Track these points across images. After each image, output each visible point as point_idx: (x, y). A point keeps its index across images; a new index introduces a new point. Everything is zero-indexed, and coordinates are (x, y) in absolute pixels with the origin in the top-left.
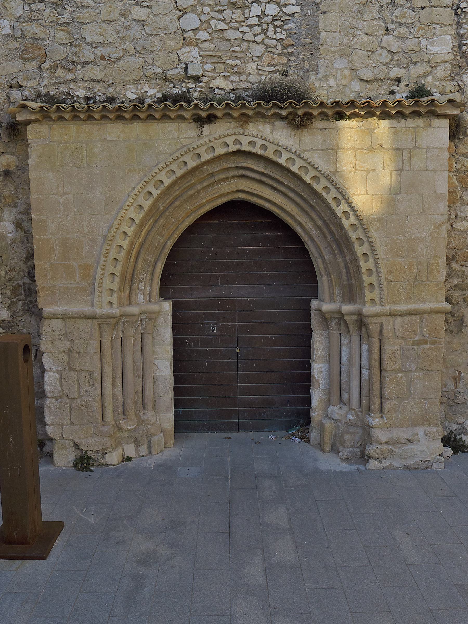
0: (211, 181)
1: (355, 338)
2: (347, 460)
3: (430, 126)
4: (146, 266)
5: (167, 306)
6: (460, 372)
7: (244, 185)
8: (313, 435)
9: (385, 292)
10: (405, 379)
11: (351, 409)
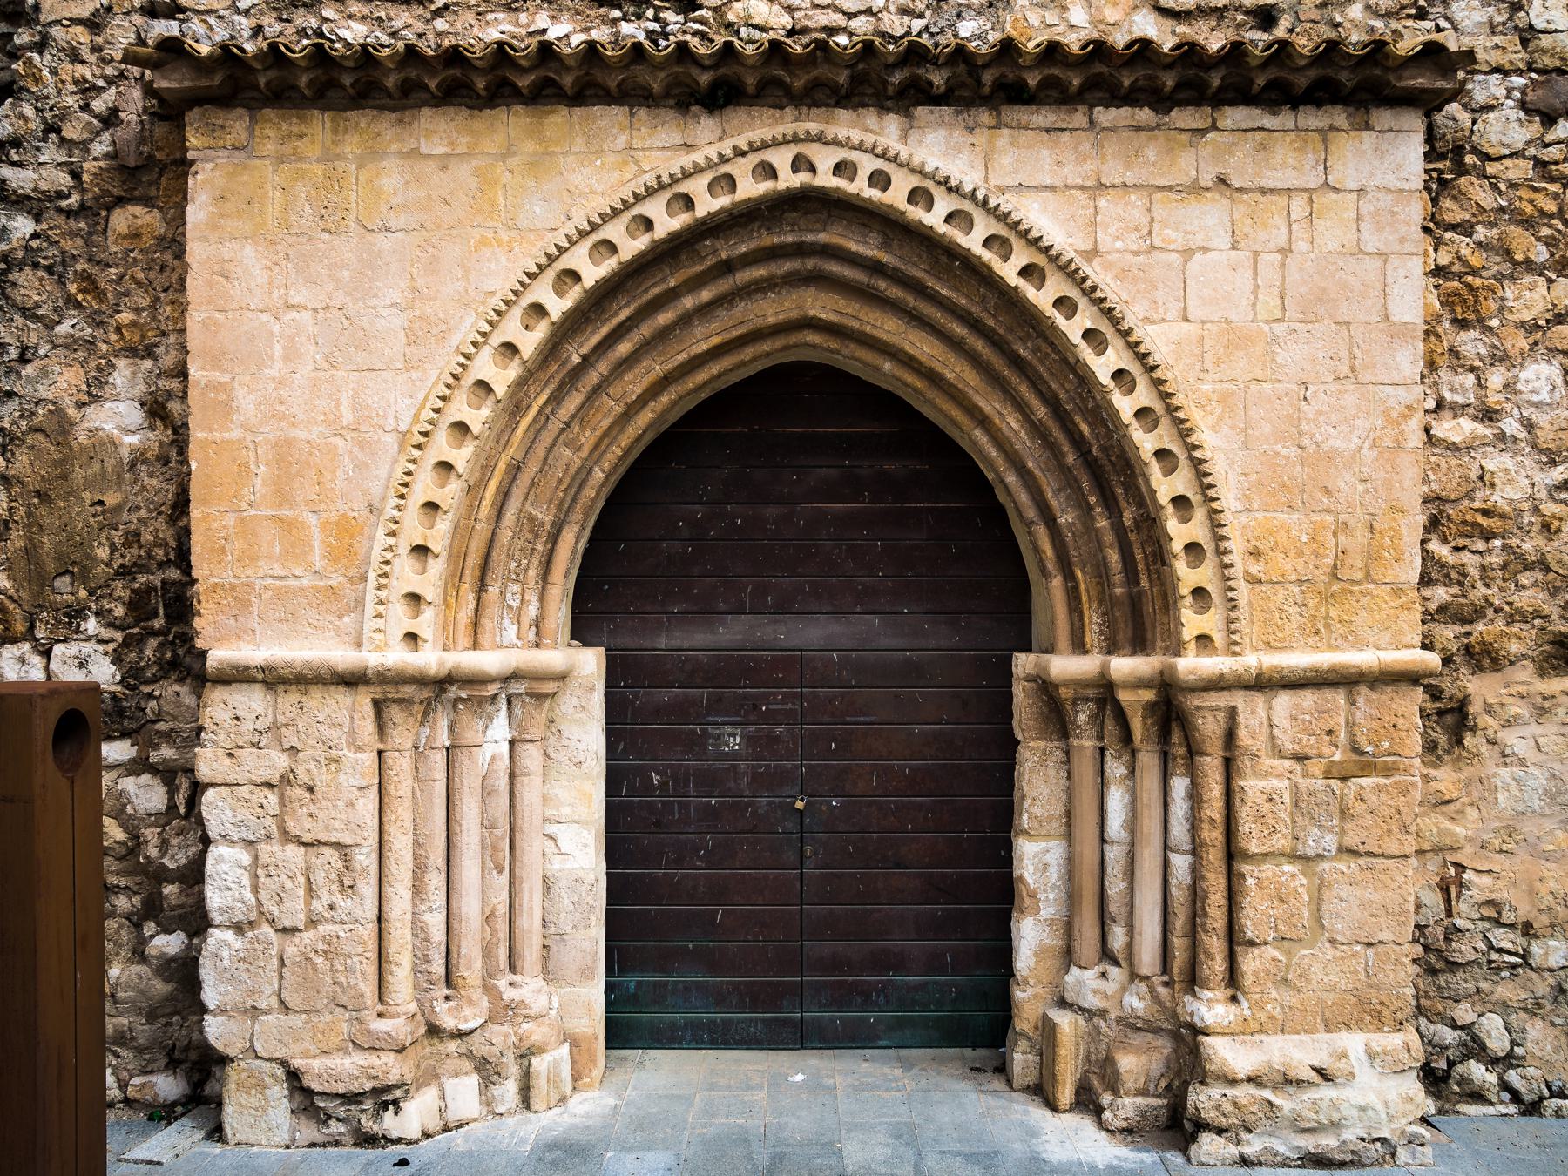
0: (724, 285)
1: (1148, 760)
2: (1128, 1132)
3: (1368, 127)
4: (529, 536)
5: (590, 663)
6: (1461, 868)
7: (820, 305)
8: (1022, 1060)
9: (1243, 613)
10: (1304, 881)
11: (1134, 976)
